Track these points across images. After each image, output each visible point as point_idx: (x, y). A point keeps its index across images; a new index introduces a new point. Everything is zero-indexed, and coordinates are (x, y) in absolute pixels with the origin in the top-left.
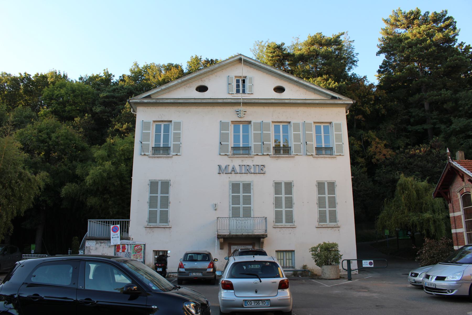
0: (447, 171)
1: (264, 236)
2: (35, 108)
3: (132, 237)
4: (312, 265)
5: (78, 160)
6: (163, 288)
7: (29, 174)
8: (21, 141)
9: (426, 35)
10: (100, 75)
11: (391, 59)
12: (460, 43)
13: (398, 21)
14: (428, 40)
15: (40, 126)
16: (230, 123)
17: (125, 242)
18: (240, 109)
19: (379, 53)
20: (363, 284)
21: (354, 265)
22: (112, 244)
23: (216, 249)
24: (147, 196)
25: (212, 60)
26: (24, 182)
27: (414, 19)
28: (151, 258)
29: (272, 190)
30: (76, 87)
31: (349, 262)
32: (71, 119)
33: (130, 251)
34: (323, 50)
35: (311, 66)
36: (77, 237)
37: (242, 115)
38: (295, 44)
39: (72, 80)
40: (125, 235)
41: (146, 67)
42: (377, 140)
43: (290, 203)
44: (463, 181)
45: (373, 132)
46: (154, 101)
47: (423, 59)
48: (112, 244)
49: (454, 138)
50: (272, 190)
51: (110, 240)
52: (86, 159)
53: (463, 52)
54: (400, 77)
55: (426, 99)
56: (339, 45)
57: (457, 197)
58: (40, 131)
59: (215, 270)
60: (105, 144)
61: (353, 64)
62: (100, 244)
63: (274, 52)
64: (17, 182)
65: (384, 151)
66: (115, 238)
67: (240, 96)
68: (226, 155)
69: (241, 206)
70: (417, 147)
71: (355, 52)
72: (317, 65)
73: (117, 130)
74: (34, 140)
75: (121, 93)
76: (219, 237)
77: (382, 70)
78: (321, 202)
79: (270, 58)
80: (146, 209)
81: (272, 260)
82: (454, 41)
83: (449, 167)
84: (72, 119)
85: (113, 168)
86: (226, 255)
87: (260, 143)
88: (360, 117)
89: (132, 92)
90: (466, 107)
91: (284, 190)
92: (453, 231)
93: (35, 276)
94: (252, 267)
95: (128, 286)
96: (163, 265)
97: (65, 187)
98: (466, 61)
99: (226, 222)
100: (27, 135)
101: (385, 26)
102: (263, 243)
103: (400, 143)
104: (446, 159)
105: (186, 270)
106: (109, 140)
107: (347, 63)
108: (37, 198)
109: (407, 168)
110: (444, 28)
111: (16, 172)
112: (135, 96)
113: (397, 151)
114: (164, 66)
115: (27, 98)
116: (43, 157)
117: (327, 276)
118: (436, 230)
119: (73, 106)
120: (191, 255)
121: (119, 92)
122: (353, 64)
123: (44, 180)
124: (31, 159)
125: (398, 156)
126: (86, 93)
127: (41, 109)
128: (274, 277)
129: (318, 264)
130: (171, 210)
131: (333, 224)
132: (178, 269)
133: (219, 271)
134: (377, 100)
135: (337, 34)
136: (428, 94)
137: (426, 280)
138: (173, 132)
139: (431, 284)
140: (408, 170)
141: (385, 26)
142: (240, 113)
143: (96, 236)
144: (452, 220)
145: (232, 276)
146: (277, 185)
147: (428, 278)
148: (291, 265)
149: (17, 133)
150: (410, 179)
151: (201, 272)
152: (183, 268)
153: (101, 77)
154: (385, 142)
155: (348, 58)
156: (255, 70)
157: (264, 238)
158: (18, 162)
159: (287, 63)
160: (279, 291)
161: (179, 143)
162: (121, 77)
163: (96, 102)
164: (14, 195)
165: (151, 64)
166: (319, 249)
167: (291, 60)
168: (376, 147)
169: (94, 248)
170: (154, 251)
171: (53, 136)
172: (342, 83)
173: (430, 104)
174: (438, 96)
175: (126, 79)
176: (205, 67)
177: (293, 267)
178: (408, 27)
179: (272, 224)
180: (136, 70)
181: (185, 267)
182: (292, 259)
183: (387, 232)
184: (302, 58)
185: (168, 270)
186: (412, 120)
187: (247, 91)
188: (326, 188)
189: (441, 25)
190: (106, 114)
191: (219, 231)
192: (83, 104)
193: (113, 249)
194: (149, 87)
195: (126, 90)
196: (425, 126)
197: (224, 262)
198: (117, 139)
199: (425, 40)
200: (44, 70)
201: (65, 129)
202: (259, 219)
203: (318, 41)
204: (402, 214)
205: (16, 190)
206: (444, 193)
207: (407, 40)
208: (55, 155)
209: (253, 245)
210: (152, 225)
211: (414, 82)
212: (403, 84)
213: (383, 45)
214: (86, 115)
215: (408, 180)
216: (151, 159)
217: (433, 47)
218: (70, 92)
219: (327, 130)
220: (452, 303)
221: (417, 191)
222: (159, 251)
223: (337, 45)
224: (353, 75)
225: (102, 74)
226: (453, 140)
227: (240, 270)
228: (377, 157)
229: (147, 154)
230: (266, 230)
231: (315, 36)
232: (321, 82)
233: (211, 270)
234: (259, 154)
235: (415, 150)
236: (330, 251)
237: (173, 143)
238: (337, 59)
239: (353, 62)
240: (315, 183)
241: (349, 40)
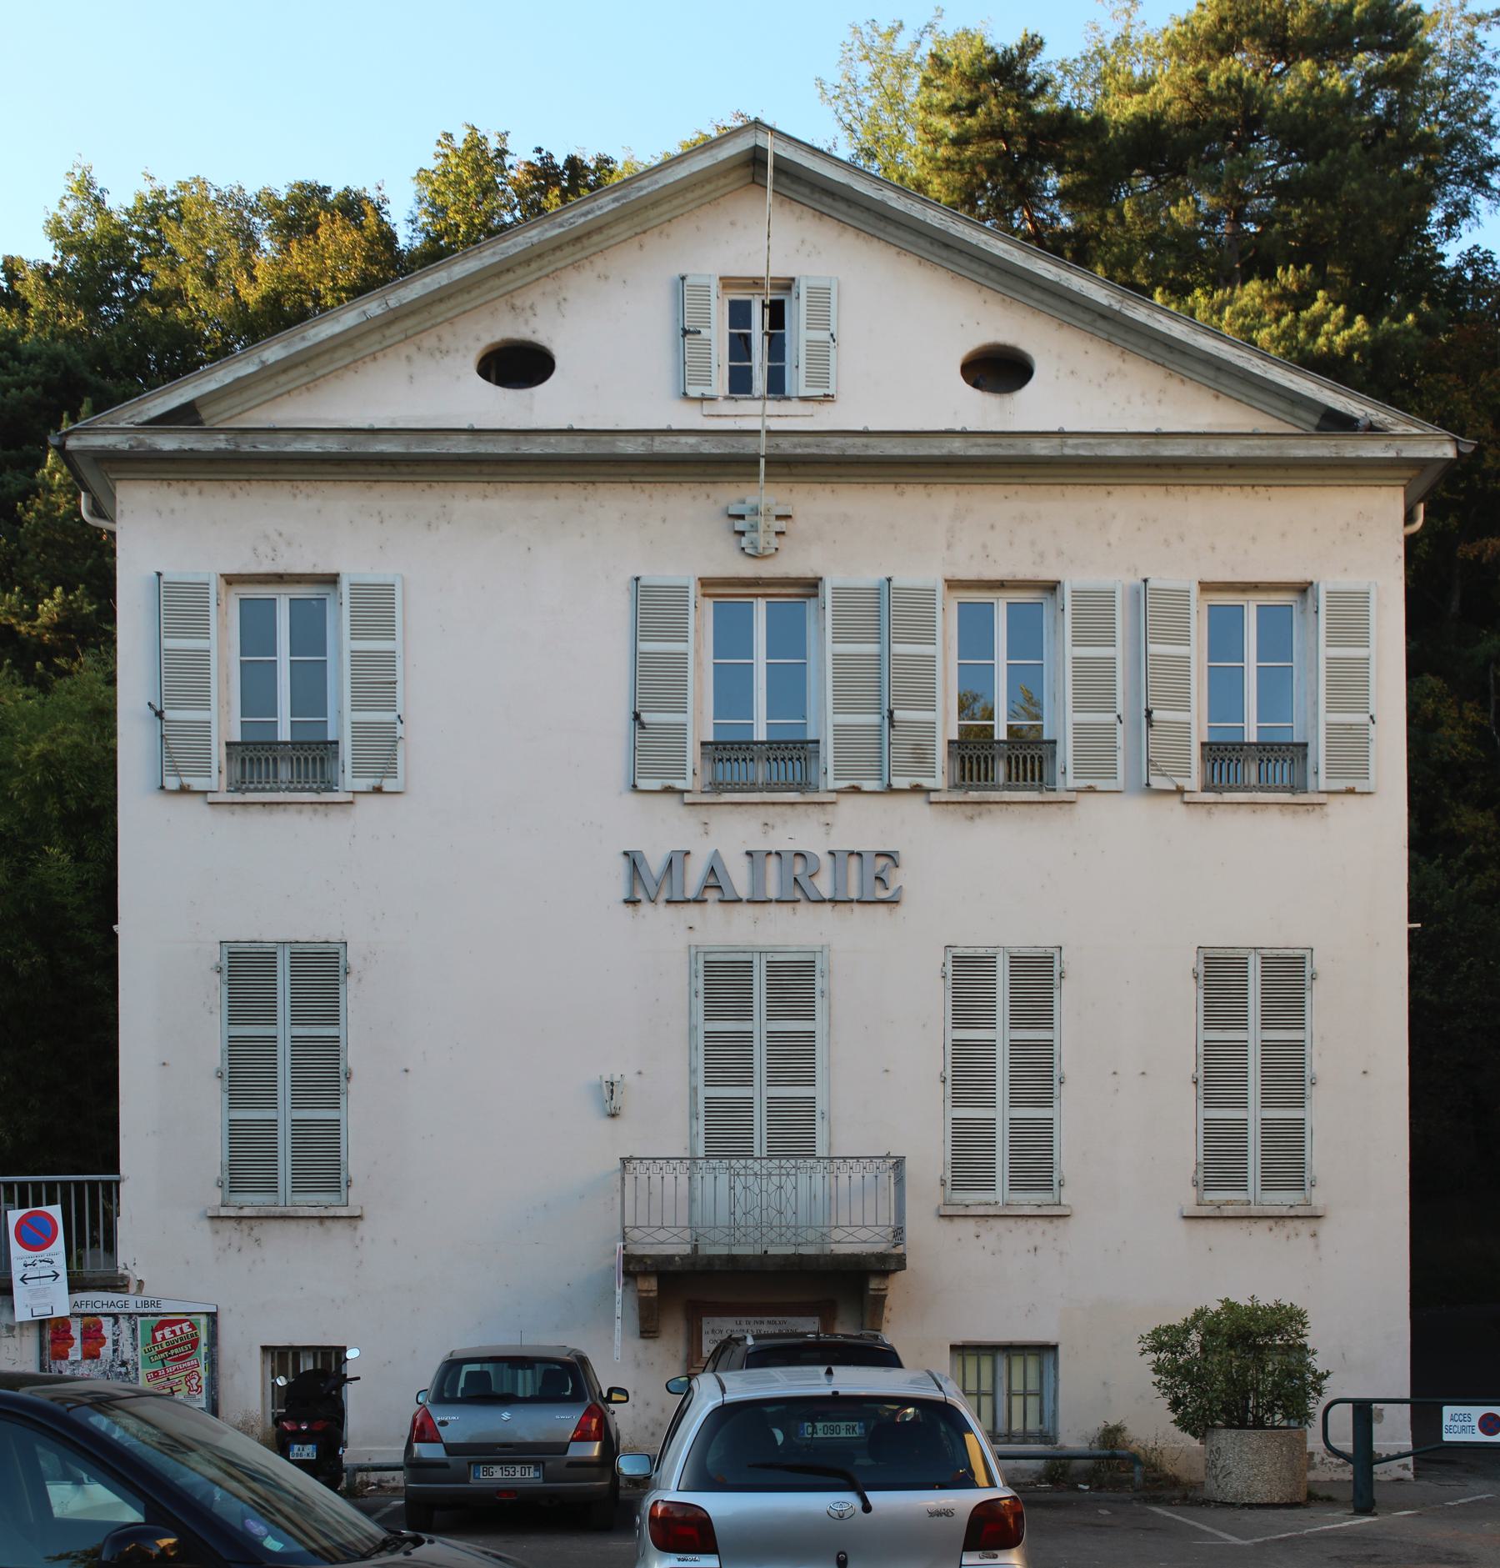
1: (888, 1264)
3: (135, 1274)
4: (1152, 1425)
6: (325, 1543)
16: (694, 591)
18: (751, 500)
21: (1394, 1432)
22: (22, 1314)
23: (618, 1335)
24: (210, 1035)
25: (572, 162)
28: (249, 1390)
29: (937, 999)
31: (1364, 1412)
33: (127, 1353)
34: (1289, 86)
35: (1206, 201)
37: (765, 540)
38: (1109, 41)
40: (93, 1263)
41: (155, 210)
43: (1037, 1074)
46: (220, 443)
48: (22, 1314)
50: (934, 998)
56: (1399, 46)
59: (611, 1450)
63: (971, 109)
67: (754, 415)
69: (760, 1092)
72: (1247, 197)
76: (634, 1267)
78: (1218, 1075)
79: (942, 152)
80: (209, 1114)
81: (931, 1393)
86: (675, 1370)
87: (874, 719)
91: (1009, 999)
94: (821, 1430)
95: (124, 1534)
99: (675, 1183)
102: (880, 1301)
105: (451, 1449)
107: (1442, 181)
112: (97, 409)
114: (268, 204)
117: (1234, 1487)
120: (476, 1367)
122: (1483, 185)
128: (943, 1487)
129: (1184, 1424)
130: (361, 1117)
132: (409, 1449)
133: (633, 1451)
138: (349, 645)
142: (754, 528)
145: (704, 1480)
146: (968, 973)
148: (1033, 1425)
151: (536, 1463)
152: (436, 1439)
155: (1455, 138)
157: (885, 1274)
159: (1053, 182)
161: (389, 717)
165: (184, 186)
166: (1195, 1337)
167: (1079, 165)
170: (265, 1349)
172: (1398, 318)
175: (29, 287)
176: (528, 214)
177: (1046, 1437)
179: (937, 1196)
180: (90, 226)
181: (448, 1435)
182: (1044, 1394)
184: (1156, 148)
185: (351, 1455)
187: (797, 380)
188: (1252, 993)
191: (635, 1234)
194: (181, 352)
197: (661, 1406)
202: (858, 1167)
222: (297, 1351)
223: (1384, 49)
227: (750, 1447)
229: (197, 783)
230: (899, 1232)
232: (1259, 314)
233: (594, 1449)
234: (868, 785)
236: (1260, 1349)
237: (349, 716)
238: (1380, 148)
240: (1191, 961)
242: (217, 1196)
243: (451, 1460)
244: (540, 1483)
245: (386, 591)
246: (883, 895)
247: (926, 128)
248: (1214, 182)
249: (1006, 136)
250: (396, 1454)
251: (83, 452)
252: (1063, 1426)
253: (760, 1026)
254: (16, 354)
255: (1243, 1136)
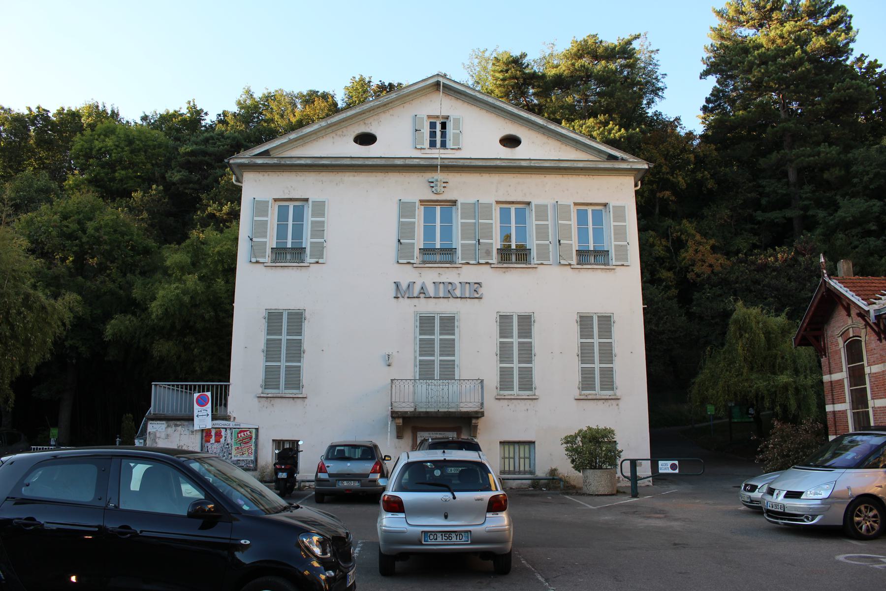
0: (819, 296)
1: (479, 415)
2: (58, 175)
3: (233, 415)
4: (566, 469)
5: (137, 272)
6: (267, 507)
7: (43, 298)
8: (29, 236)
9: (794, 40)
10: (181, 112)
11: (727, 86)
12: (858, 56)
13: (743, 13)
14: (797, 50)
15: (65, 208)
16: (418, 203)
17: (220, 423)
18: (436, 178)
19: (705, 74)
20: (659, 504)
21: (645, 470)
22: (196, 427)
24: (262, 338)
25: (390, 84)
26: (33, 312)
27: (772, 10)
28: (268, 456)
29: (495, 329)
30: (135, 133)
31: (634, 463)
32: (126, 194)
33: (229, 441)
34: (599, 67)
35: (577, 97)
36: (130, 415)
39: (128, 122)
41: (268, 98)
42: (698, 237)
43: (527, 353)
44: (849, 315)
45: (690, 222)
46: (275, 161)
47: (788, 87)
48: (196, 427)
49: (841, 236)
51: (193, 420)
52: (152, 269)
53: (864, 74)
54: (743, 119)
55: (791, 161)
57: (837, 345)
58: (65, 217)
60: (188, 241)
61: (657, 94)
62: (174, 428)
63: (507, 71)
64: (19, 313)
65: (711, 259)
66: (203, 418)
67: (437, 153)
68: (409, 263)
69: (437, 358)
70: (770, 251)
71: (660, 71)
73: (212, 216)
74: (54, 233)
75: (219, 146)
76: (395, 415)
77: (710, 105)
78: (585, 353)
80: (259, 363)
82: (847, 52)
83: (823, 289)
84: (127, 194)
85: (201, 287)
87: (474, 242)
88: (667, 193)
89: (238, 146)
90: (866, 178)
91: (517, 329)
92: (829, 408)
93: (28, 485)
95: (197, 503)
96: (288, 467)
97: (112, 321)
98: (868, 91)
99: (409, 388)
100: (40, 225)
101: (717, 22)
102: (476, 427)
103: (742, 243)
104: (820, 276)
105: (330, 475)
106: (195, 234)
107: (645, 93)
108: (58, 343)
109: (751, 291)
110: (828, 27)
111: (17, 294)
113: (733, 259)
115: (43, 154)
116: (71, 265)
117: (592, 489)
118: (799, 407)
119: (130, 171)
121: (215, 144)
122: (657, 94)
123: (71, 310)
124: (49, 268)
125: (736, 267)
126: (155, 145)
127: (70, 176)
129: (577, 468)
130: (307, 365)
131: (607, 393)
134: (701, 161)
135: (627, 37)
136: (794, 152)
137: (768, 498)
138: (311, 219)
139: (777, 505)
140: (753, 294)
141: (717, 22)
142: (436, 185)
143: (169, 412)
144: (827, 388)
145: (402, 488)
146: (504, 320)
147: (772, 495)
148: (527, 468)
149: (23, 220)
150: (754, 311)
151: (358, 481)
152: (326, 472)
153: (181, 115)
154: (712, 242)
155: (647, 82)
156: (465, 105)
157: (478, 418)
158: (22, 275)
159: (531, 91)
160: (489, 515)
161: (322, 240)
162: (220, 115)
163: (173, 163)
164: (14, 336)
165: (276, 91)
166: (579, 439)
167: (539, 87)
168: (696, 251)
169: (163, 436)
170: (273, 440)
171: (90, 226)
172: (635, 129)
173: (800, 171)
174: (814, 156)
175: (229, 119)
177: (532, 472)
178: (761, 26)
179: (495, 393)
180: (249, 102)
182: (531, 458)
183: (711, 409)
184: (560, 82)
186: (764, 201)
187: (450, 144)
188: (595, 327)
189: (823, 21)
190: (191, 185)
191: (394, 404)
192: (149, 166)
193: (198, 437)
194: (272, 134)
195: (229, 141)
196: (789, 213)
198: (209, 234)
199: (791, 50)
200: (75, 102)
201: (113, 214)
202: (468, 382)
203: (589, 50)
204: (737, 376)
205: (18, 326)
206: (814, 337)
207: (758, 49)
208: (93, 262)
209: (459, 430)
210: (271, 392)
211: (769, 129)
212: (749, 132)
213: (713, 60)
214: (154, 186)
215: (751, 314)
216: (269, 270)
217: (807, 63)
218: (123, 144)
219: (598, 219)
220: (812, 539)
221: (767, 334)
222: (284, 441)
223: (625, 59)
224: (656, 115)
225: (184, 111)
226: (840, 238)
227: (419, 477)
228: (696, 269)
229: (261, 260)
230: (482, 404)
231: (585, 41)
234: (471, 262)
235: (766, 258)
239: (656, 91)
240: (576, 317)
241: (650, 49)
242: (260, 390)
243: (330, 479)
244: (359, 487)
245: (323, 203)
246: (477, 296)
247: (493, 76)
248: (578, 91)
249: (517, 79)
250: (312, 477)
251: (234, 164)
252: (537, 469)
253: (437, 337)
254: (223, 137)
255: (594, 373)
